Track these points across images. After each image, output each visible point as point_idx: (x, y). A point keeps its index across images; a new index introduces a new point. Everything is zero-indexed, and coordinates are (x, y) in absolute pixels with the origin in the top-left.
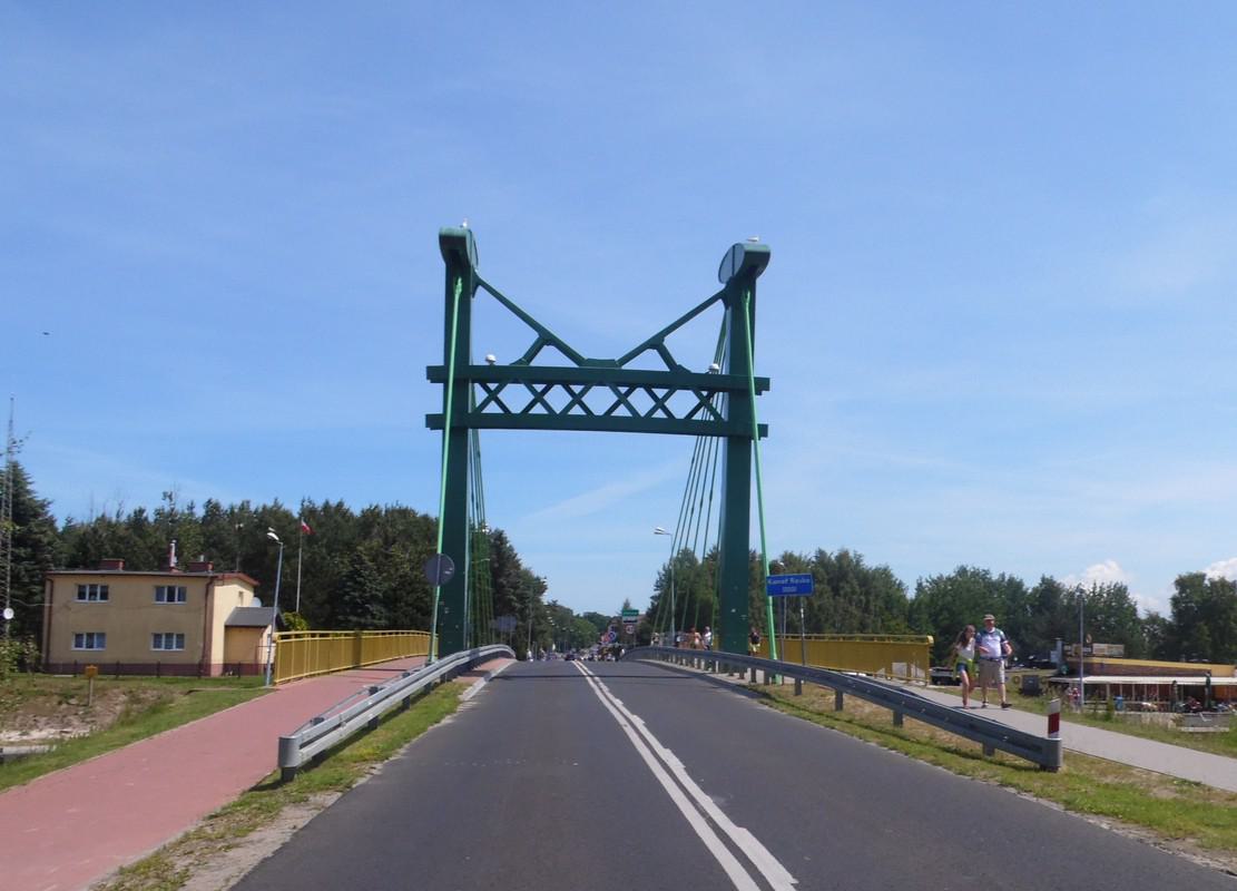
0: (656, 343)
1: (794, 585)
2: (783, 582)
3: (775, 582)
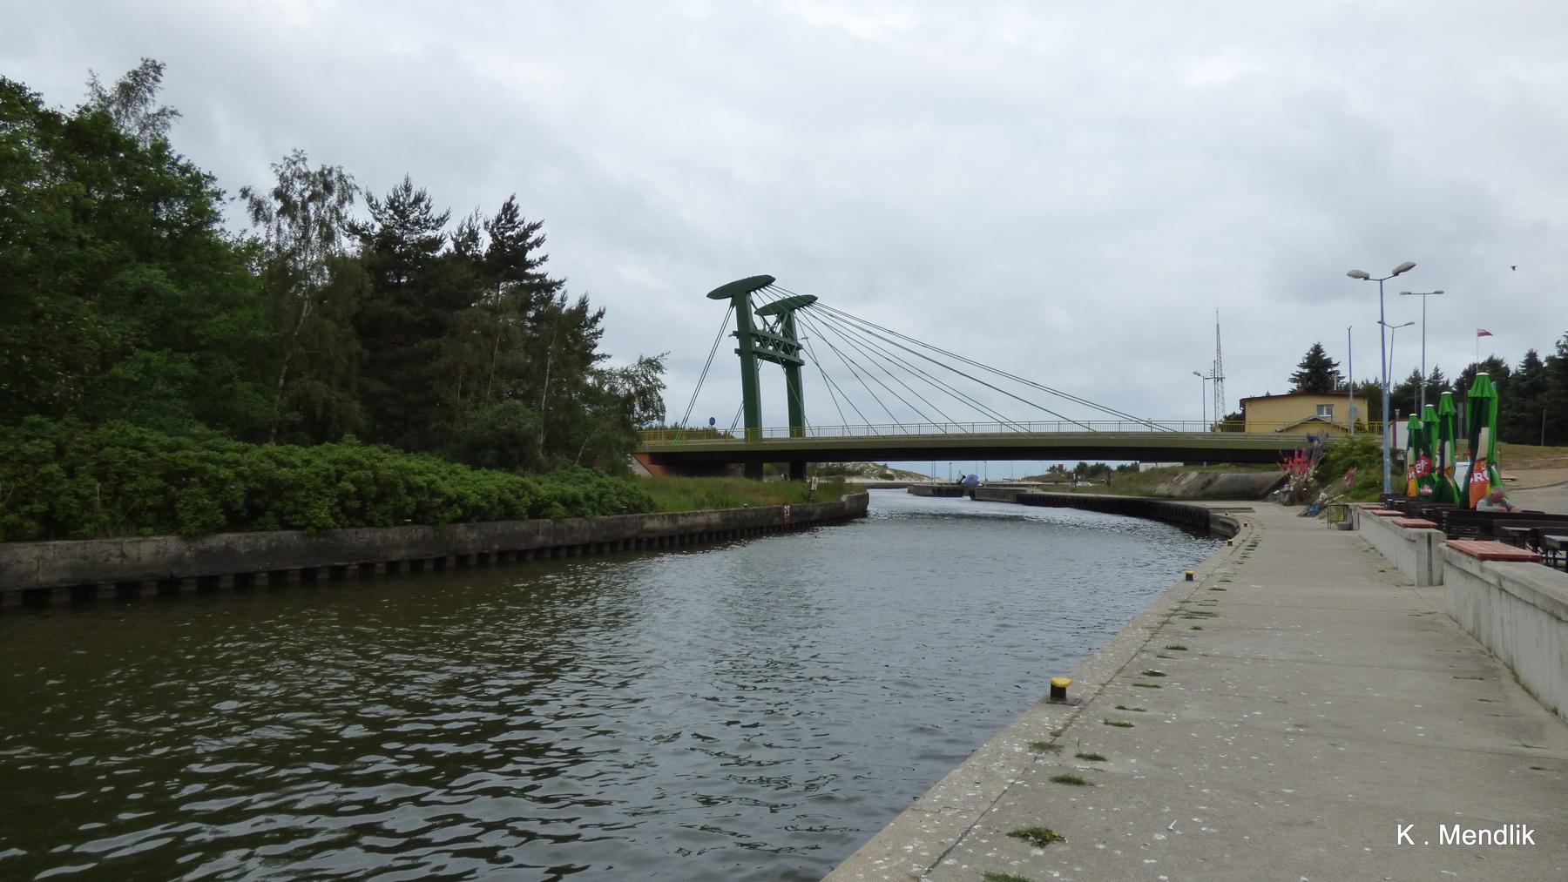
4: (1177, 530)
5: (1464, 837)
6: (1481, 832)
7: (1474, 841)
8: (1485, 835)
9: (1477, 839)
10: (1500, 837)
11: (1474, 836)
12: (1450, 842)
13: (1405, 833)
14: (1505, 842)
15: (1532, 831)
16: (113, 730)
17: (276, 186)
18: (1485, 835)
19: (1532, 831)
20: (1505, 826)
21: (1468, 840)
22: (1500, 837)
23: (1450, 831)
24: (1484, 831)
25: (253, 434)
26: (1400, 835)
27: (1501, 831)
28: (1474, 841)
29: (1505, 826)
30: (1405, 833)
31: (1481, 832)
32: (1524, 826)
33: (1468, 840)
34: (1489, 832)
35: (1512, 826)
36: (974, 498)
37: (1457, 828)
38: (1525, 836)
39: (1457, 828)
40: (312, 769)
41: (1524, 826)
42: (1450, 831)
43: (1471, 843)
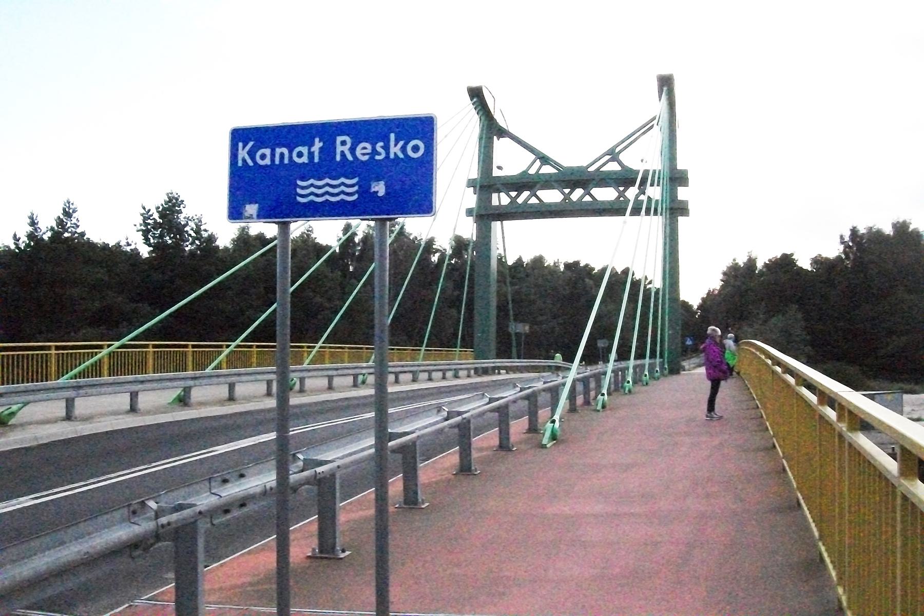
0: (613, 155)
1: (347, 168)
2: (302, 155)
3: (264, 158)
8: (282, 155)
18: (282, 155)
34: (285, 151)
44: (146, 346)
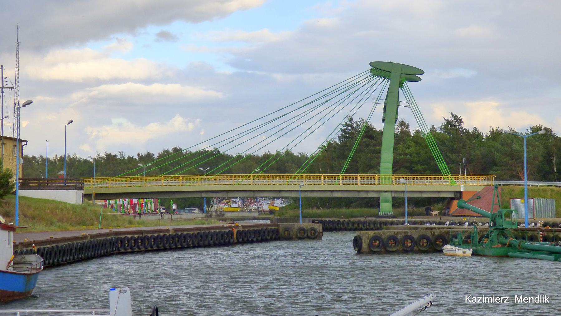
4: (335, 232)
5: (524, 300)
6: (530, 298)
7: (527, 301)
9: (529, 301)
10: (537, 300)
11: (500, 300)
12: (519, 302)
13: (468, 298)
14: (486, 298)
15: (548, 298)
16: (221, 286)
17: (277, 200)
19: (548, 298)
20: (539, 296)
21: (525, 301)
22: (537, 300)
23: (519, 298)
24: (531, 298)
25: (342, 218)
26: (466, 299)
27: (537, 298)
28: (499, 301)
29: (539, 296)
30: (468, 298)
31: (530, 298)
32: (545, 296)
33: (525, 301)
34: (491, 298)
35: (541, 296)
36: (495, 171)
37: (521, 297)
38: (546, 300)
39: (521, 297)
40: (201, 289)
41: (545, 296)
42: (519, 298)
43: (527, 302)
44: (180, 176)
